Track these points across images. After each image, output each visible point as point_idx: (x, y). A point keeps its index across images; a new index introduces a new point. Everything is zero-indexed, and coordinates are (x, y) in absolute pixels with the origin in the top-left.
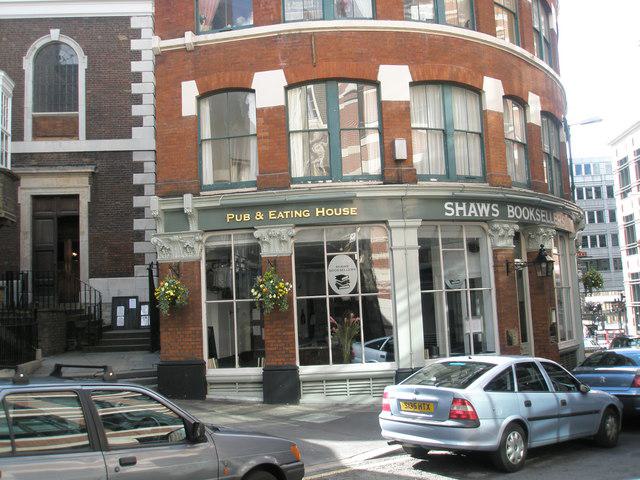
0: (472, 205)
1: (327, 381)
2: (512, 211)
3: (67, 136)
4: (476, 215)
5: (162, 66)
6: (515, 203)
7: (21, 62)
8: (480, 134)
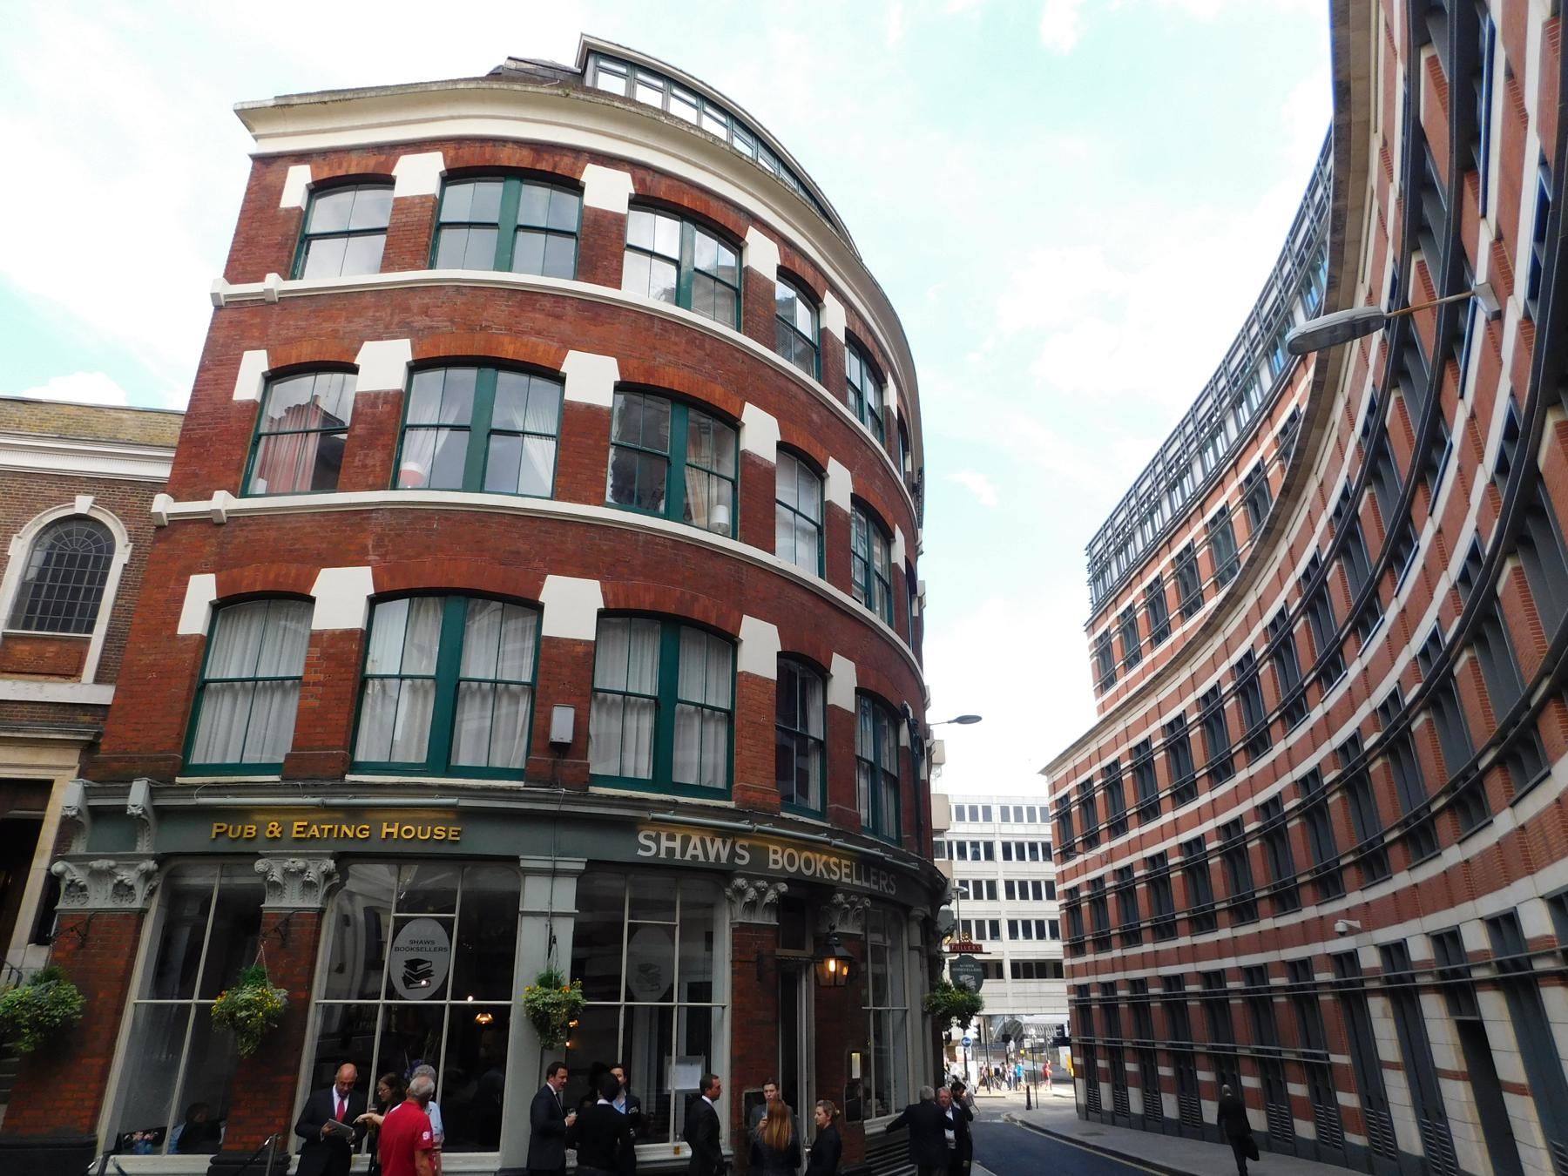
3: (60, 675)
4: (701, 858)
5: (163, 546)
8: (729, 715)
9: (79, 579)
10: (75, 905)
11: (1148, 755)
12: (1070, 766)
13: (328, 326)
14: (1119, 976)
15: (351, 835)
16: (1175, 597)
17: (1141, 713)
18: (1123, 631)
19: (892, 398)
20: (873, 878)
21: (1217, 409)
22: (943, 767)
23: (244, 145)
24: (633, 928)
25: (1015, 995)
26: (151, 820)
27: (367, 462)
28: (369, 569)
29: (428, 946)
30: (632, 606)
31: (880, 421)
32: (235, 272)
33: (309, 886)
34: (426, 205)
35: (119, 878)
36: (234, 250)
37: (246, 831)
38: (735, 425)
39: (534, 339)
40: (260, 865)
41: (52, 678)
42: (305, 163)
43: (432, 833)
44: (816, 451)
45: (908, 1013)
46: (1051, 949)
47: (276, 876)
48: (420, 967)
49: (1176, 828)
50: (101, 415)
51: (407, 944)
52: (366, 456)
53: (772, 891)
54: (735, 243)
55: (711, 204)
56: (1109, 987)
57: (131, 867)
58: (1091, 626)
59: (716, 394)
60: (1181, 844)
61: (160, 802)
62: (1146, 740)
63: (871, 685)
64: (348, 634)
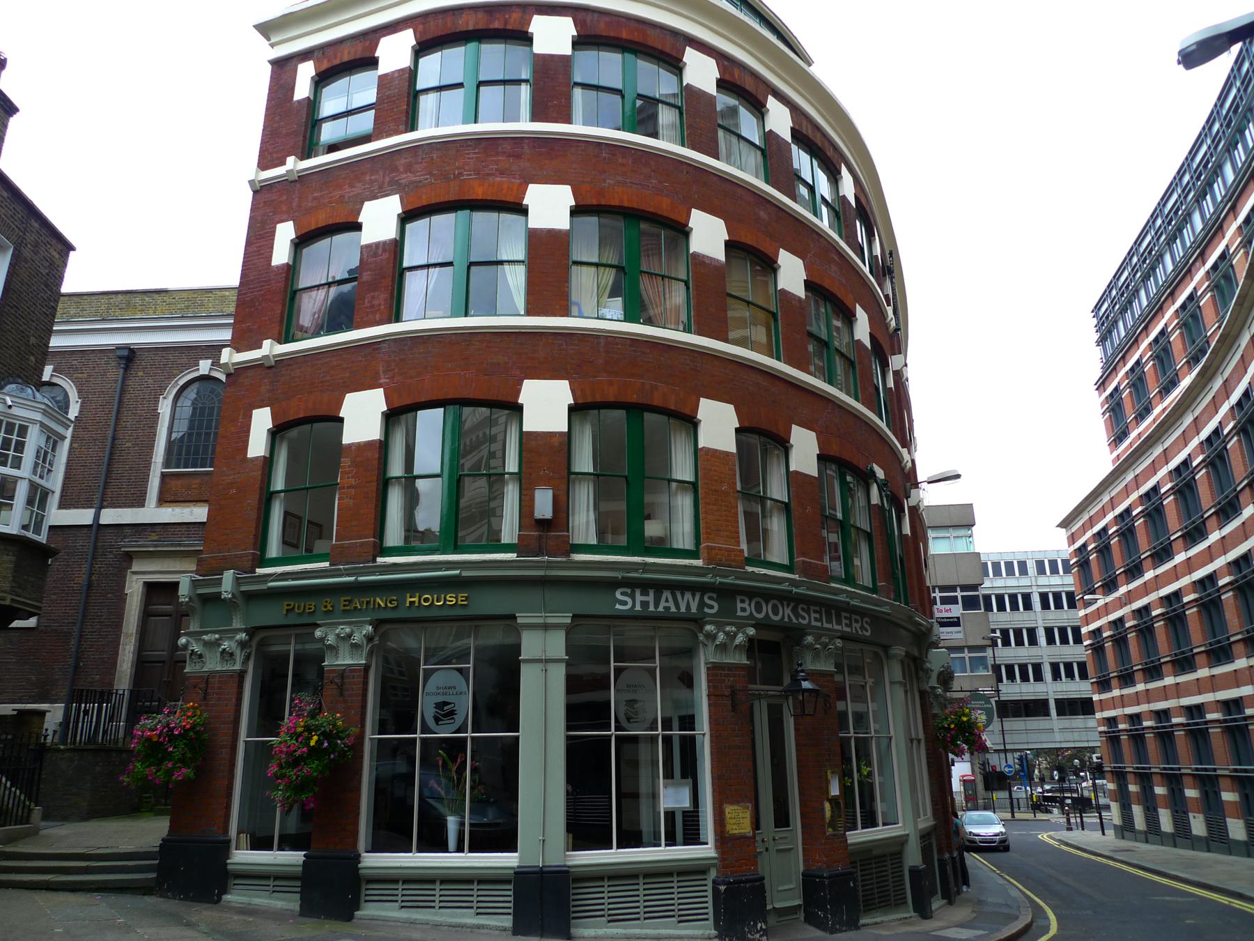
0: (667, 594)
1: (480, 882)
2: (744, 608)
4: (673, 609)
6: (750, 593)
7: (157, 402)
8: (694, 486)
9: (209, 427)
10: (197, 668)
11: (1157, 500)
12: (1086, 517)
13: (337, 193)
14: (1144, 708)
15: (382, 604)
16: (1181, 347)
17: (1149, 461)
18: (1133, 385)
19: (848, 188)
20: (844, 621)
21: (1212, 156)
22: (974, 528)
23: (265, 52)
24: (618, 671)
25: (1062, 730)
26: (240, 601)
27: (374, 303)
28: (381, 390)
29: (451, 691)
30: (598, 399)
31: (839, 210)
32: (266, 161)
33: (355, 646)
34: (404, 77)
35: (223, 647)
36: (263, 142)
37: (308, 607)
38: (683, 231)
39: (498, 179)
40: (318, 633)
41: (199, 504)
42: (309, 60)
43: (445, 600)
44: (764, 246)
45: (893, 740)
46: (1079, 688)
47: (331, 640)
48: (445, 708)
49: (1189, 565)
50: (210, 295)
51: (434, 690)
52: (373, 297)
53: (741, 635)
54: (675, 65)
55: (648, 32)
56: (1135, 719)
57: (231, 638)
58: (1101, 385)
59: (663, 205)
60: (1194, 582)
61: (243, 588)
62: (1155, 486)
63: (834, 450)
64: (370, 444)
